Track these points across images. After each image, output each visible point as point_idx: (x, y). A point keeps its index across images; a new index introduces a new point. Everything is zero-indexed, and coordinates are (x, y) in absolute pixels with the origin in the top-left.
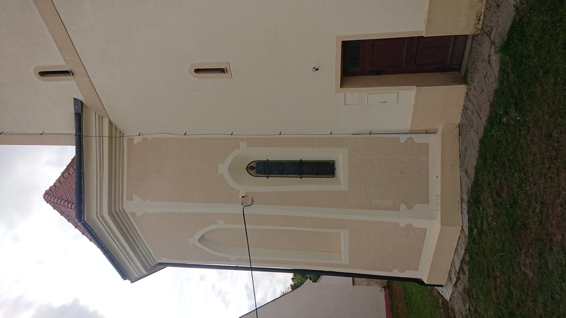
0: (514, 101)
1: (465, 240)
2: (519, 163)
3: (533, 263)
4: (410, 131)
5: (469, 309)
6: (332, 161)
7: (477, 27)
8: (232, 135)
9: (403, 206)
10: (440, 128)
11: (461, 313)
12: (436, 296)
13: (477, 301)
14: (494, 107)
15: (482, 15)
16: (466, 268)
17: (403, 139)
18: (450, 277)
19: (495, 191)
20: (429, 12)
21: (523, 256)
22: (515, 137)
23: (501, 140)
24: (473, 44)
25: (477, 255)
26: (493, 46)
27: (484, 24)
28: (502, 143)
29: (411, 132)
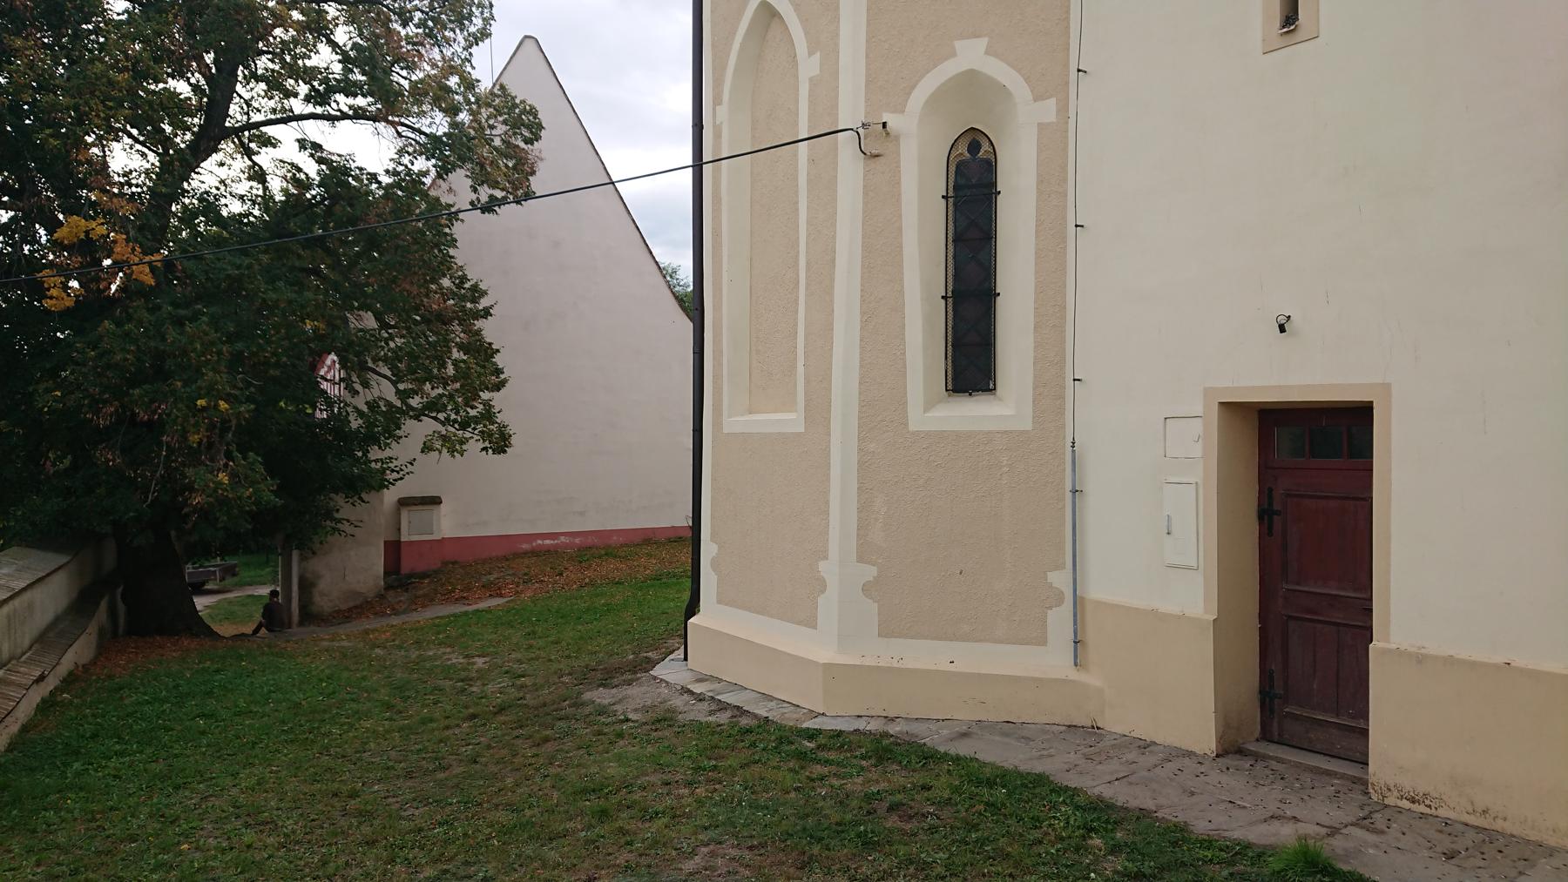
0: (1148, 871)
1: (789, 718)
2: (971, 865)
3: (716, 874)
4: (1082, 598)
5: (628, 720)
6: (995, 384)
7: (1389, 793)
8: (1079, 70)
9: (871, 572)
10: (1091, 679)
11: (620, 701)
12: (665, 645)
13: (642, 739)
14: (1138, 818)
15: (1427, 811)
16: (723, 718)
17: (1060, 579)
18: (707, 680)
19: (904, 801)
20: (1450, 661)
21: (734, 852)
22: (1044, 864)
23: (1041, 827)
24: (1336, 778)
25: (751, 745)
26: (1323, 831)
27: (1400, 812)
28: (1031, 828)
29: (1078, 602)
